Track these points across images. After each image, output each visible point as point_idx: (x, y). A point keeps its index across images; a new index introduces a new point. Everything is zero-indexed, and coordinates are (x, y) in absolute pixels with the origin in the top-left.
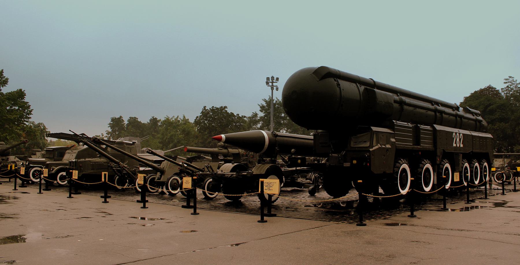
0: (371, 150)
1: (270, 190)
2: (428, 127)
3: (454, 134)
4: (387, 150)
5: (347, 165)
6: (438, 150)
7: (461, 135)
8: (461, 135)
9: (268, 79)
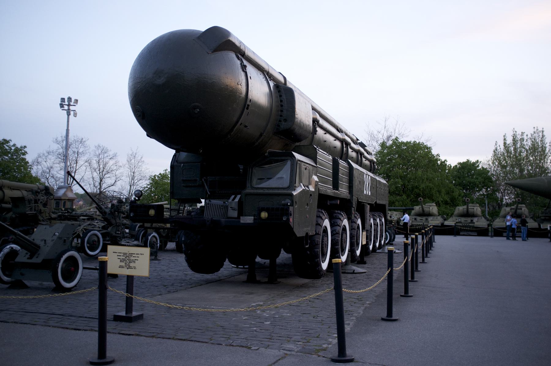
1: (130, 267)
5: (248, 220)
9: (63, 100)
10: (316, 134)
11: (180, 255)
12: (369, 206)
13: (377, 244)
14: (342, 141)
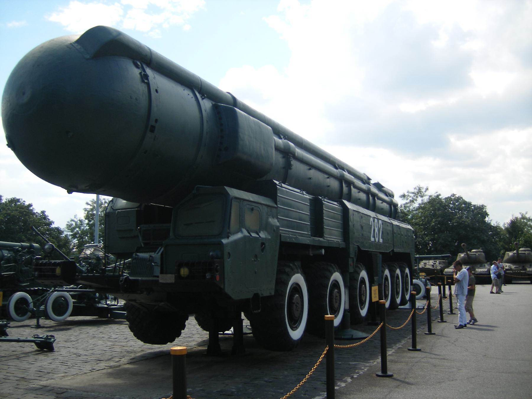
0: (224, 241)
2: (335, 205)
3: (372, 219)
4: (263, 244)
6: (351, 246)
7: (380, 222)
8: (380, 222)
10: (291, 169)
11: (114, 328)
12: (381, 256)
13: (398, 300)
14: (341, 179)
